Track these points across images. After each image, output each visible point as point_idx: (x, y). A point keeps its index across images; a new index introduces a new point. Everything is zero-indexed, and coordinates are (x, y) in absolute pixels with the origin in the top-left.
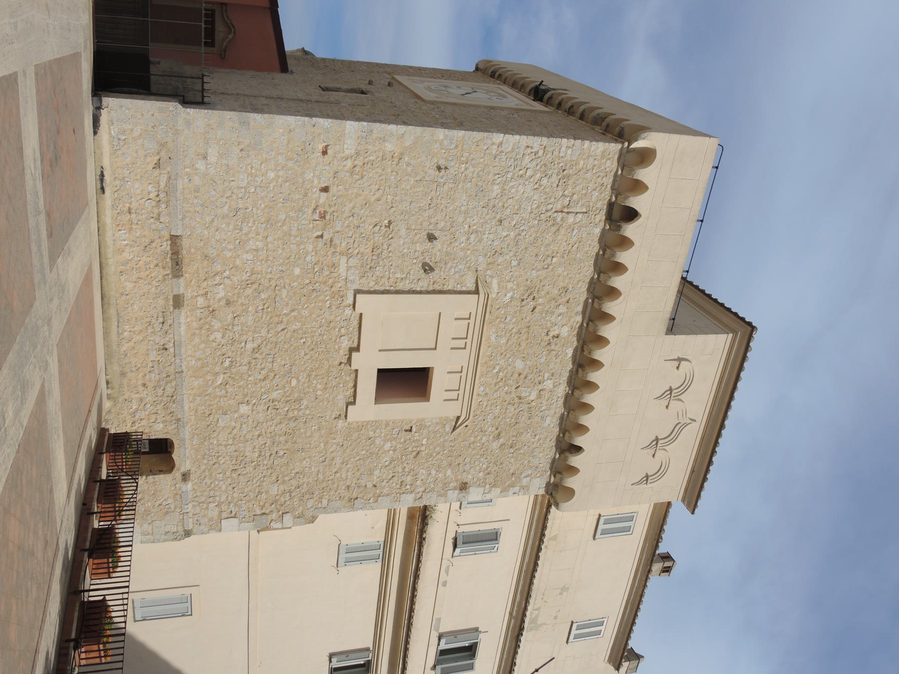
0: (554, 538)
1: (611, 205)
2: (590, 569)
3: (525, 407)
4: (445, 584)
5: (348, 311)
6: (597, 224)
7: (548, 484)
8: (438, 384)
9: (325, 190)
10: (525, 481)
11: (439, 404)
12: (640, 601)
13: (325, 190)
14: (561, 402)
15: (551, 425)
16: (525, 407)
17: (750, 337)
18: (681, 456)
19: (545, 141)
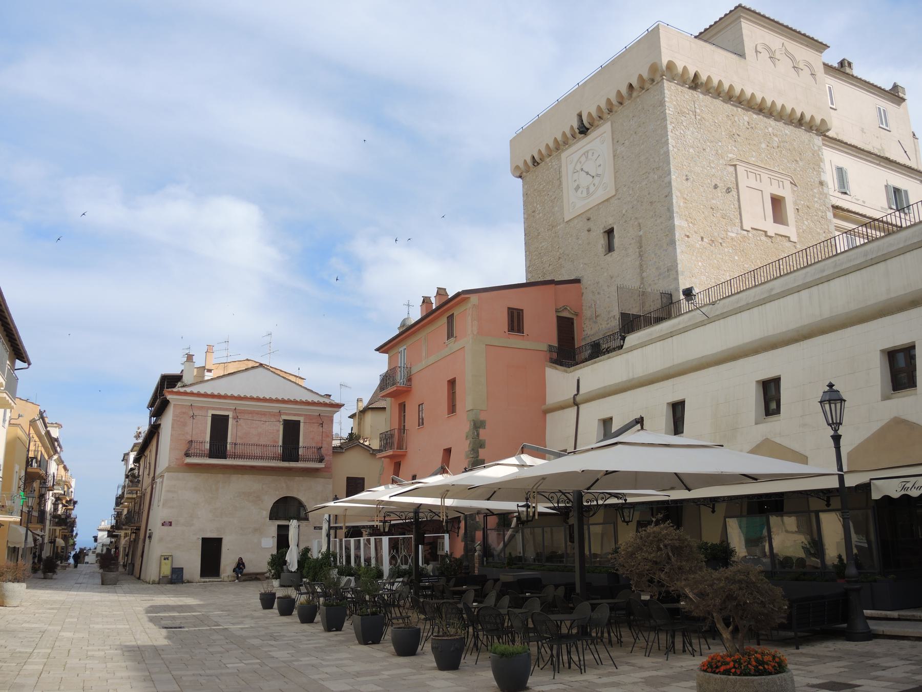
0: (837, 134)
1: (690, 88)
2: (850, 113)
3: (782, 144)
4: (864, 202)
5: (750, 235)
6: (698, 96)
7: (817, 135)
8: (779, 192)
9: (702, 238)
10: (816, 148)
11: (786, 192)
12: (868, 83)
13: (702, 238)
14: (778, 123)
15: (789, 130)
16: (782, 144)
17: (744, 8)
18: (803, 53)
19: (668, 122)
